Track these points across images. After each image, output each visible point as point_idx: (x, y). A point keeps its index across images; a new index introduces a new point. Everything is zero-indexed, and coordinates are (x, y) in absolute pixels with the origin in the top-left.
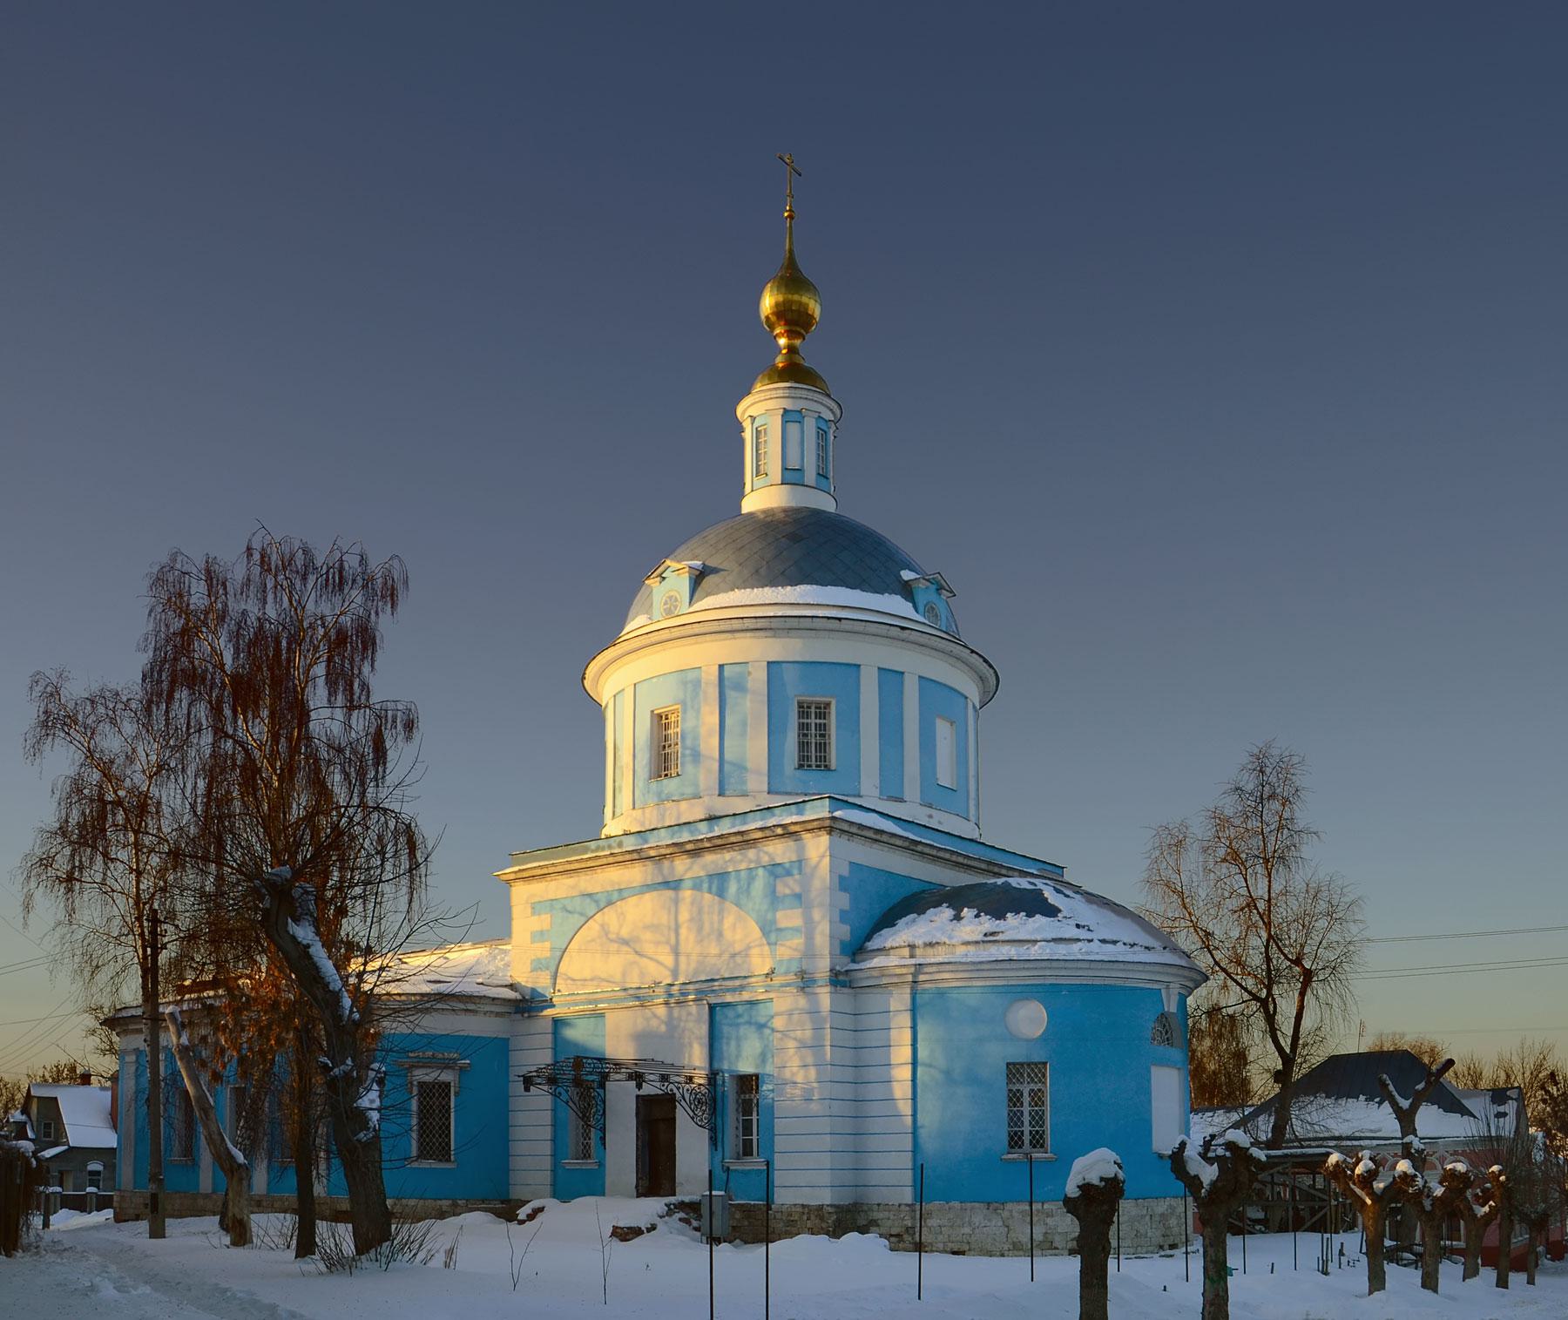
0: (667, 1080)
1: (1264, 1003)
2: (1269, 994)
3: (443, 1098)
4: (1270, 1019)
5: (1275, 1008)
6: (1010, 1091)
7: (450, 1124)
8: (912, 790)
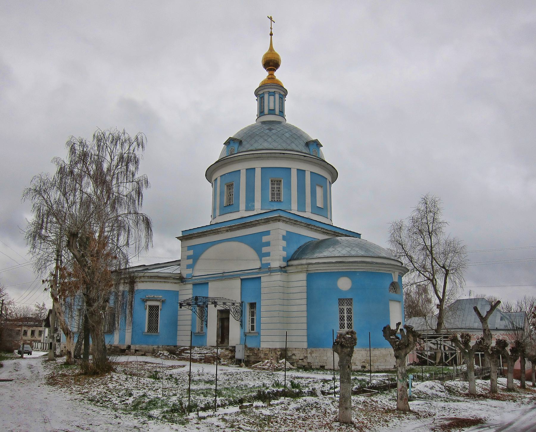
0: (225, 304)
1: (432, 281)
2: (434, 277)
3: (157, 311)
4: (435, 286)
5: (436, 283)
6: (340, 308)
7: (158, 319)
8: (308, 208)
